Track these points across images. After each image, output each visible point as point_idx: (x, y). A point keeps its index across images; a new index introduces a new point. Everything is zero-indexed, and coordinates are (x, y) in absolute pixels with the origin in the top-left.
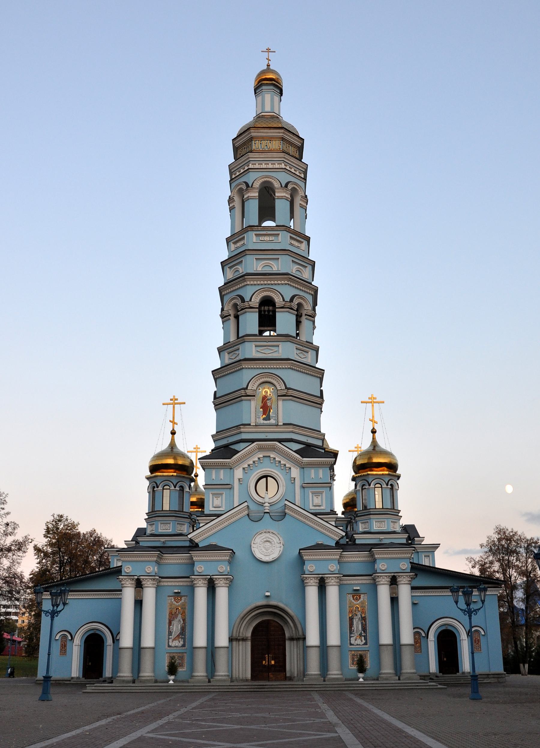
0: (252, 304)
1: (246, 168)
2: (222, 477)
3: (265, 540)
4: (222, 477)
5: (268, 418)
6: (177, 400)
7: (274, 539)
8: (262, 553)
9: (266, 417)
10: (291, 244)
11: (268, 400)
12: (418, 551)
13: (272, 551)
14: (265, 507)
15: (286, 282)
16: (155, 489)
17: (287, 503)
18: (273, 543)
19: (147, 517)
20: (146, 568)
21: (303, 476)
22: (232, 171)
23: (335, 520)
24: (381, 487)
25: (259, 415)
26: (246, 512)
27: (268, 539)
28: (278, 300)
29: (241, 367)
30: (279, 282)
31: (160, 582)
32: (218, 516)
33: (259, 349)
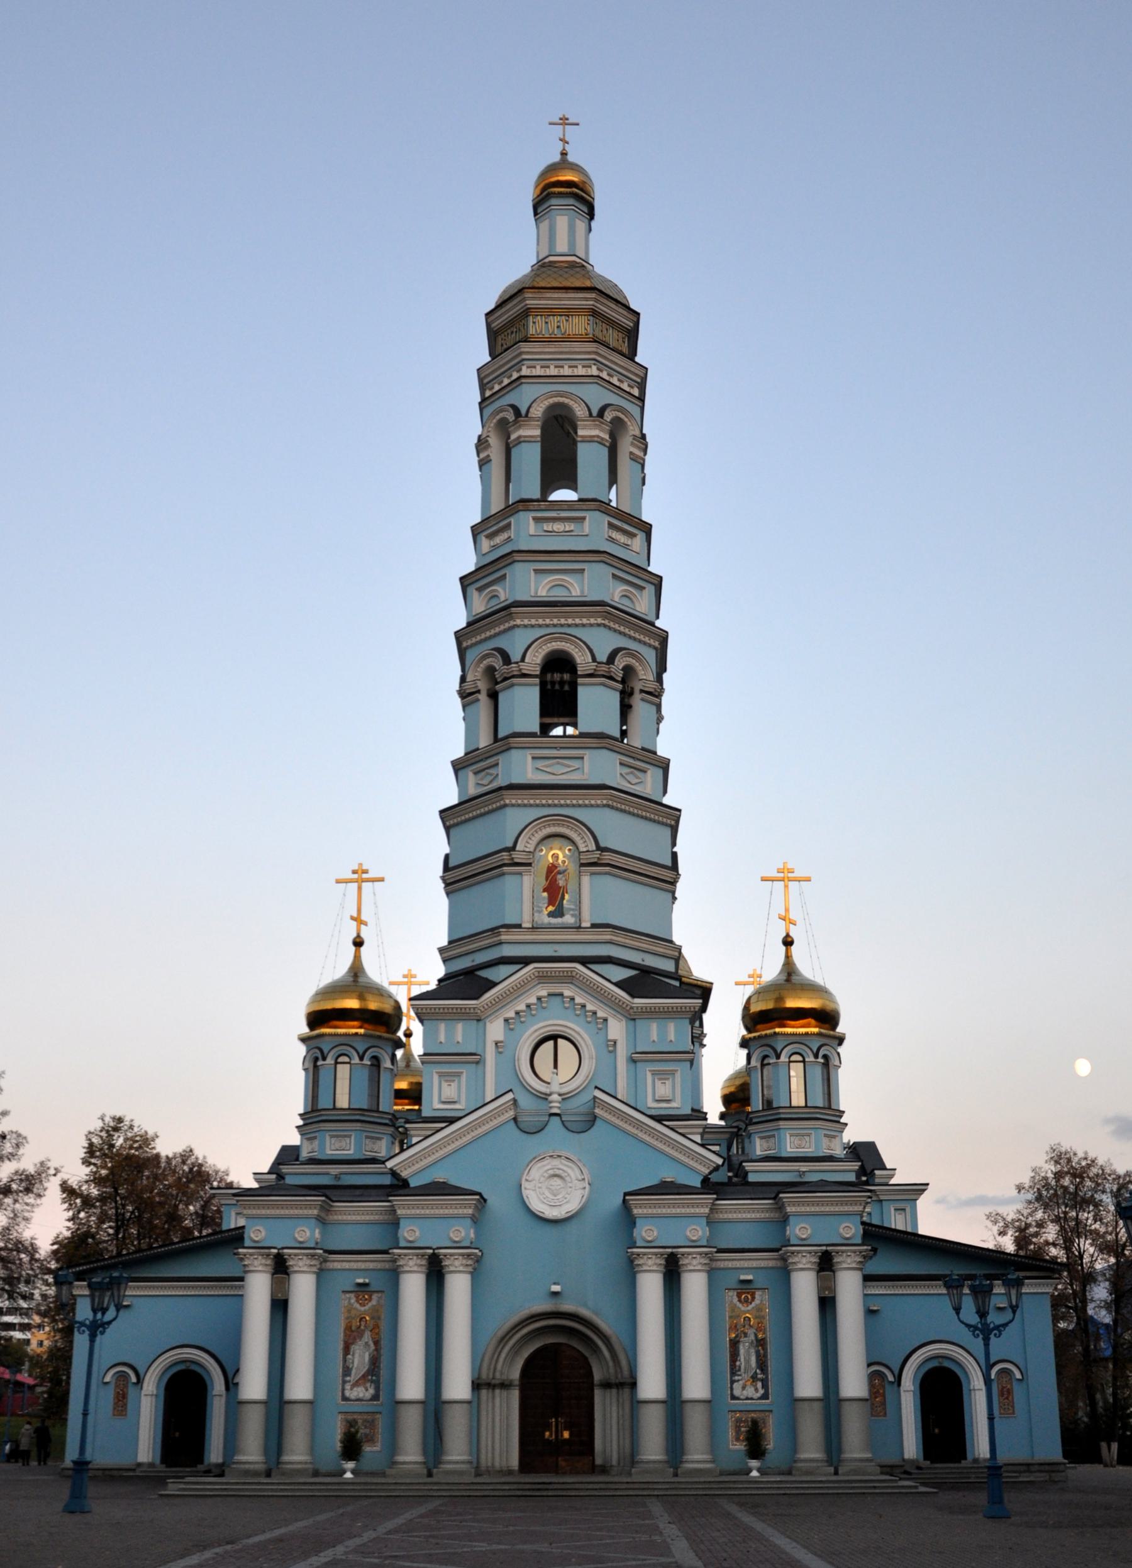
0: (526, 668)
1: (515, 375)
2: (672, 1037)
3: (551, 1172)
4: (672, 1037)
5: (559, 912)
6: (366, 872)
7: (569, 1171)
8: (545, 1201)
9: (555, 910)
10: (611, 540)
11: (559, 873)
12: (882, 1198)
13: (567, 1196)
14: (551, 1102)
15: (600, 621)
16: (320, 1063)
17: (598, 1094)
18: (568, 1179)
19: (301, 1123)
20: (296, 1231)
21: (633, 1036)
22: (485, 381)
23: (701, 1130)
24: (804, 1061)
25: (540, 905)
26: (511, 1114)
27: (558, 1172)
28: (582, 660)
29: (502, 802)
30: (585, 621)
31: (325, 1261)
32: (451, 1121)
33: (540, 764)
